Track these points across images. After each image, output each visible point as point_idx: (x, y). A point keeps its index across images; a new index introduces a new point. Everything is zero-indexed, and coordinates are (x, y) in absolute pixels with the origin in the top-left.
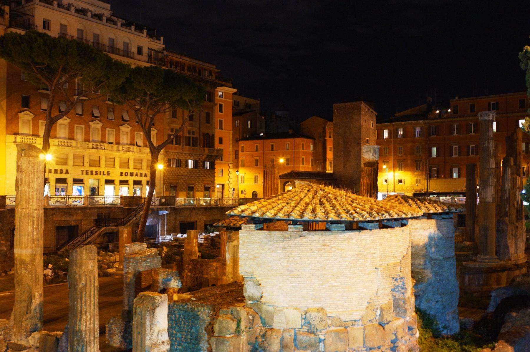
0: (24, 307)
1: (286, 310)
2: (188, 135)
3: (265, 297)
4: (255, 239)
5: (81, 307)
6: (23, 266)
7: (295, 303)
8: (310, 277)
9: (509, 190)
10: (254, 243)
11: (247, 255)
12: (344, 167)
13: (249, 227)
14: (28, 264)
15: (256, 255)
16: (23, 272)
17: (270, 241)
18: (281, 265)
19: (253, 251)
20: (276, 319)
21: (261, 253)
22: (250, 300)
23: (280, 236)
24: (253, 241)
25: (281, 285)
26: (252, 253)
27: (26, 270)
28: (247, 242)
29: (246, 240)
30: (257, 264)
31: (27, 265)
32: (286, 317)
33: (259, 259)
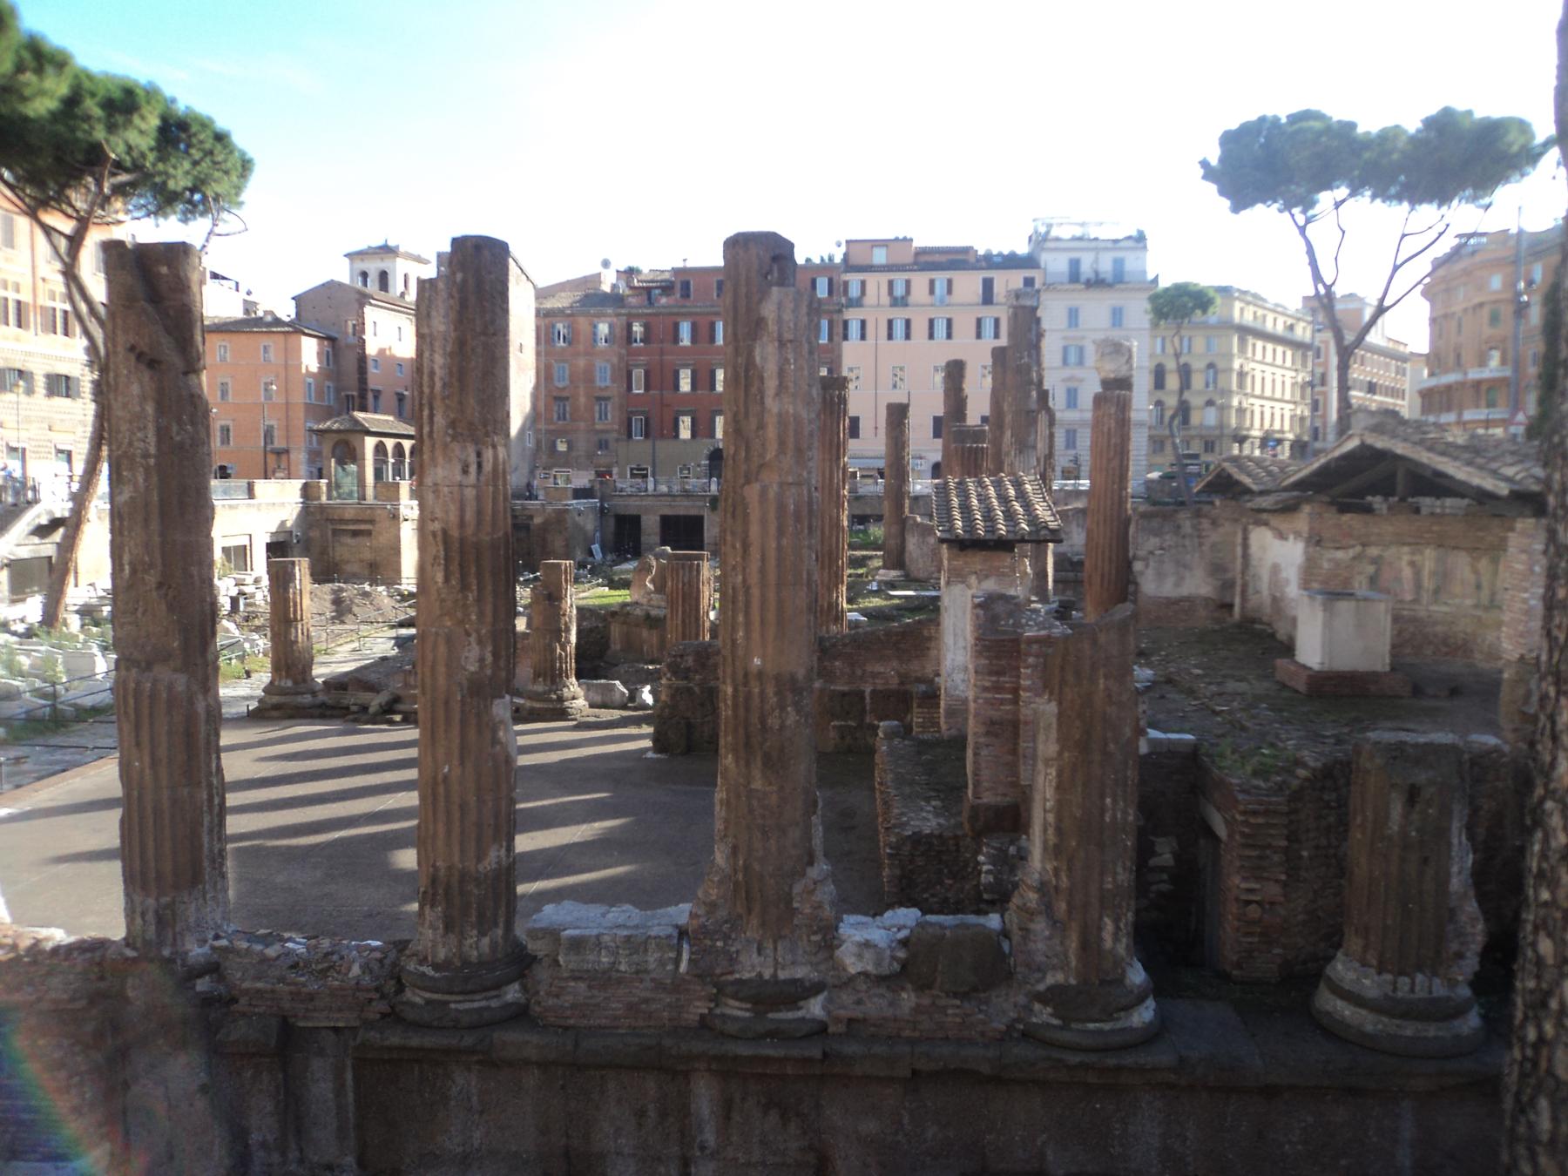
2: (50, 304)
16: (788, 722)
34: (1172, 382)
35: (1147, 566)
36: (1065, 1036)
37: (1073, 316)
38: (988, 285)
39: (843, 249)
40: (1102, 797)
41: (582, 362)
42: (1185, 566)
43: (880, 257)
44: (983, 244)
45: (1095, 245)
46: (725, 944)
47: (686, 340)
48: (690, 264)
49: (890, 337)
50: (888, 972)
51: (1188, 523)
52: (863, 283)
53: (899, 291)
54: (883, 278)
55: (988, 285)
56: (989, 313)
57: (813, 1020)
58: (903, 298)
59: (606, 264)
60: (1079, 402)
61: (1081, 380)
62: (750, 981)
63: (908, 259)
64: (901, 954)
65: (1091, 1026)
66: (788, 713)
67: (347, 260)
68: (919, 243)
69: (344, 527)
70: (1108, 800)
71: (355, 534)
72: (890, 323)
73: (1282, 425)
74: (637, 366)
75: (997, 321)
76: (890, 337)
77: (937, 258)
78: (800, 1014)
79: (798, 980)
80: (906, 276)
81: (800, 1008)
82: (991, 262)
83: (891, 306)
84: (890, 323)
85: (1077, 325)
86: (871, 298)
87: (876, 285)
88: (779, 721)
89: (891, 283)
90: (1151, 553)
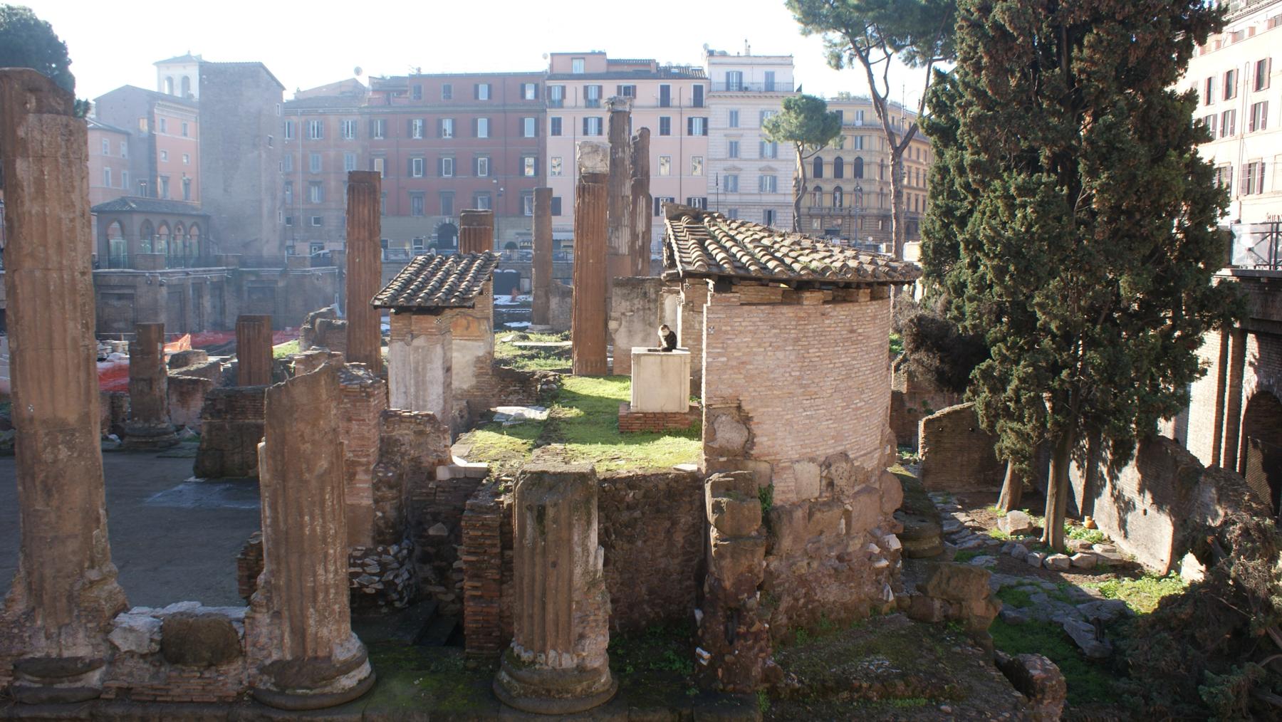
0: (74, 553)
1: (797, 466)
3: (761, 443)
4: (743, 324)
5: (323, 527)
6: (60, 437)
7: (809, 450)
8: (832, 394)
9: (643, 233)
10: (741, 332)
11: (724, 359)
12: (225, 190)
13: (728, 300)
14: (74, 430)
15: (744, 359)
16: (61, 457)
17: (773, 327)
18: (791, 375)
19: (739, 350)
20: (779, 486)
21: (755, 354)
22: (721, 456)
23: (791, 315)
24: (741, 328)
25: (789, 417)
26: (736, 354)
27: (70, 449)
28: (726, 332)
29: (724, 328)
30: (745, 377)
31: (73, 435)
32: (796, 479)
33: (751, 367)
34: (848, 172)
35: (620, 325)
36: (279, 700)
37: (734, 116)
38: (665, 91)
39: (549, 60)
40: (302, 516)
41: (332, 153)
42: (650, 324)
43: (579, 67)
44: (665, 58)
45: (752, 61)
46: (21, 631)
47: (482, 133)
48: (424, 72)
49: (690, 132)
50: (146, 651)
51: (652, 290)
52: (563, 88)
53: (593, 95)
54: (580, 85)
55: (665, 91)
56: (593, 114)
57: (92, 689)
58: (596, 101)
59: (358, 71)
60: (778, 188)
61: (740, 169)
62: (39, 659)
63: (602, 68)
64: (843, 615)
65: (300, 691)
66: (59, 450)
67: (155, 68)
68: (610, 56)
69: (111, 292)
70: (307, 518)
71: (120, 297)
72: (586, 121)
73: (916, 209)
74: (378, 156)
75: (600, 121)
76: (690, 132)
77: (626, 69)
78: (79, 685)
79: (81, 658)
80: (562, 83)
81: (80, 680)
82: (667, 73)
83: (586, 107)
84: (586, 121)
85: (736, 125)
86: (569, 101)
87: (574, 90)
88: (52, 456)
89: (586, 88)
90: (623, 314)
